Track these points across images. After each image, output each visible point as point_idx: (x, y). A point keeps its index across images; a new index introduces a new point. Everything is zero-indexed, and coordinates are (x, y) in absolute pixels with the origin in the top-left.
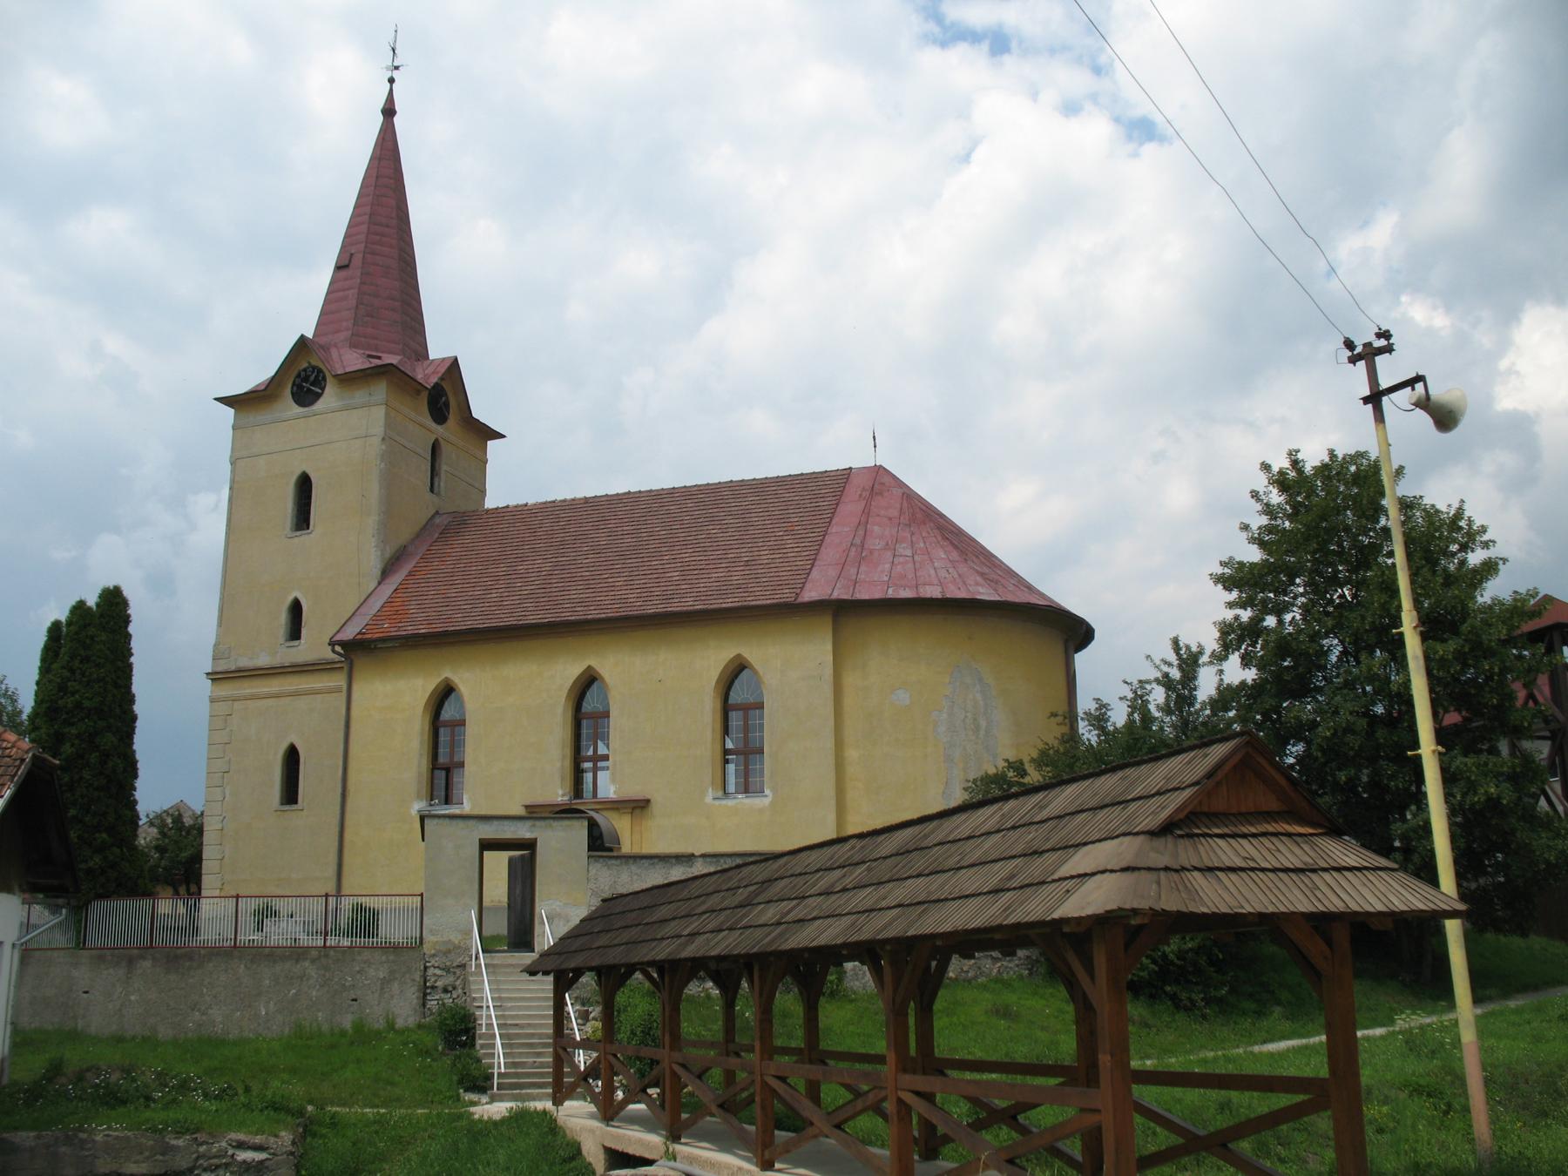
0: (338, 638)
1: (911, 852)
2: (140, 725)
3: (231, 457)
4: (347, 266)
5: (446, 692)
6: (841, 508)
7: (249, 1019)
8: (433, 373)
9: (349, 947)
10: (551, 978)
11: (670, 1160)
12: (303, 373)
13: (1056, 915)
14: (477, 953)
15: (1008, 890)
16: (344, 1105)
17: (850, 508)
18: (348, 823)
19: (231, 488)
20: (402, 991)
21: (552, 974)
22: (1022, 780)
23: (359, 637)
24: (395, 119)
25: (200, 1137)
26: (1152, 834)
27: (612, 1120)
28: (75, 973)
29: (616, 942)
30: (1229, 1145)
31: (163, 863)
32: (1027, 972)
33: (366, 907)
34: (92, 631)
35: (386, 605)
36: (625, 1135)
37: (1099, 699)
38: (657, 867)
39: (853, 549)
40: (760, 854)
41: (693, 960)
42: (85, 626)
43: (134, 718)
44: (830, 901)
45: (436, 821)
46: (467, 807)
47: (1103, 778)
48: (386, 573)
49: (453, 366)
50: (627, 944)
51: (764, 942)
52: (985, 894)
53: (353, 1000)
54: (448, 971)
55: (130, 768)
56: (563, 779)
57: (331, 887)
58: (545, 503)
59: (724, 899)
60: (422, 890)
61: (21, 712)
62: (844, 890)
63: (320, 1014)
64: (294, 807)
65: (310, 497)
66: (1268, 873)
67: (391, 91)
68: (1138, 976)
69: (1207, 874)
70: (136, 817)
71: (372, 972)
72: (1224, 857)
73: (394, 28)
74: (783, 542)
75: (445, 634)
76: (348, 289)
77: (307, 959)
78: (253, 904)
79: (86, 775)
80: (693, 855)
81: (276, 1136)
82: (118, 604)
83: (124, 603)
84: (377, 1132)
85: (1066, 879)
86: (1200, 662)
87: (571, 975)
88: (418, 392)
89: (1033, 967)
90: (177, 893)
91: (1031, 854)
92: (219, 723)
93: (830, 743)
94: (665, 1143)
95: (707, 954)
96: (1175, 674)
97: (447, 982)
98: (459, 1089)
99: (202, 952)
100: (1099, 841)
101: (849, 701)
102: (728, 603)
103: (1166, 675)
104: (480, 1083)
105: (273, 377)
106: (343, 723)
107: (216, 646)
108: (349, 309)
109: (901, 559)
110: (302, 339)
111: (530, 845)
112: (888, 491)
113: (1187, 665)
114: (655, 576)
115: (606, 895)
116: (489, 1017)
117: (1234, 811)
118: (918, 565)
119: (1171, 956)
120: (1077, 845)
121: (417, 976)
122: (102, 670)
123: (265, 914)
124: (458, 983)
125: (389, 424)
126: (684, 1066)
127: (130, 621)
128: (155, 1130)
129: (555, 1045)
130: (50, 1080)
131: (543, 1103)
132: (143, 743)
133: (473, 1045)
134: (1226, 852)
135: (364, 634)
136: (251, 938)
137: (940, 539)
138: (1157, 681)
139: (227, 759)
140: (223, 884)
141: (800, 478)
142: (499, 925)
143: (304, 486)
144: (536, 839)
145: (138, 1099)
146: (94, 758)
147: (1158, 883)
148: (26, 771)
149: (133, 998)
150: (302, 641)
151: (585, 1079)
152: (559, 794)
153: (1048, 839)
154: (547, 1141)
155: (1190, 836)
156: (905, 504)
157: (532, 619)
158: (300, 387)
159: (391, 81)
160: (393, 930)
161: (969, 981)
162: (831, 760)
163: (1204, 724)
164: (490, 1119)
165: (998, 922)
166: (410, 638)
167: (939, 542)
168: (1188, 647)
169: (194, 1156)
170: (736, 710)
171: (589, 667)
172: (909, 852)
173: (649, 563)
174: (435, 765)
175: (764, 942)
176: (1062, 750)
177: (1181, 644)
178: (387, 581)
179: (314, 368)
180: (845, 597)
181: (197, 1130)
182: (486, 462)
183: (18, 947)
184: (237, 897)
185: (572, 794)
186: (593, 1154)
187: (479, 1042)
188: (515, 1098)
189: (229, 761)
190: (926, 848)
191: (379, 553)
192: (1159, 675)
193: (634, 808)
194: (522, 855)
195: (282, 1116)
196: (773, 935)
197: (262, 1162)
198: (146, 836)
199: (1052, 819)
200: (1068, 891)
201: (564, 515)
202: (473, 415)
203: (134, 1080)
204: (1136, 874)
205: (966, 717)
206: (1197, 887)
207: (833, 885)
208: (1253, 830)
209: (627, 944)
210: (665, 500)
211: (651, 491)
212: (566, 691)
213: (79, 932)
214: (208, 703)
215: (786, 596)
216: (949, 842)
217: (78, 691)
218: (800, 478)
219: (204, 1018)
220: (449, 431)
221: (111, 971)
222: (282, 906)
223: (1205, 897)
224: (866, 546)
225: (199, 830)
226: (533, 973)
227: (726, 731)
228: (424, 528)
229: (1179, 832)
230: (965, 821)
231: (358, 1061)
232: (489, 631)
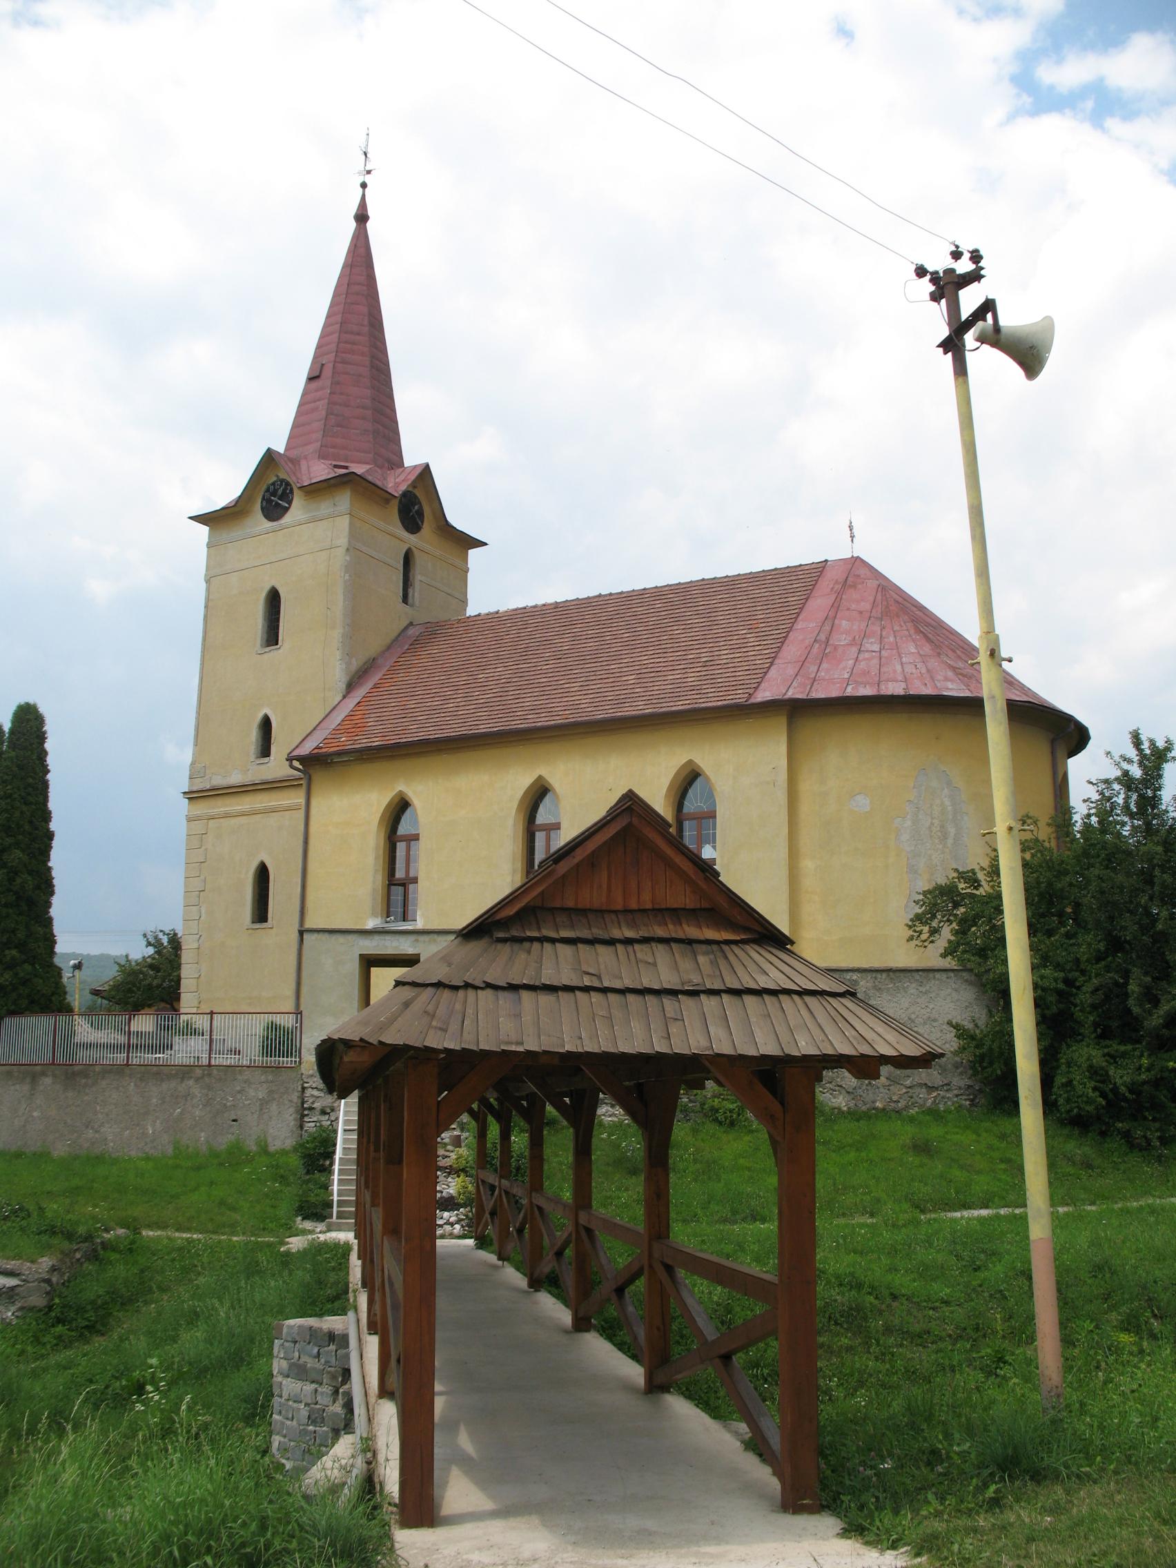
5: (401, 807)
6: (810, 603)
7: (137, 1138)
9: (248, 1067)
12: (272, 487)
17: (820, 603)
20: (280, 1112)
22: (975, 892)
23: (316, 751)
24: (368, 225)
32: (968, 1103)
33: (284, 1028)
35: (347, 718)
39: (817, 646)
43: (50, 836)
45: (315, 936)
46: (420, 924)
48: (350, 687)
49: (425, 473)
53: (234, 1121)
58: (516, 610)
63: (203, 1134)
64: (264, 925)
65: (278, 612)
71: (252, 1093)
73: (366, 132)
74: (746, 641)
75: (397, 746)
76: (319, 400)
77: (191, 1077)
88: (387, 501)
89: (975, 1097)
92: (196, 841)
93: (783, 852)
96: (1136, 772)
101: (806, 808)
103: (1126, 773)
105: (240, 497)
107: (193, 764)
109: (867, 655)
112: (863, 583)
114: (611, 680)
117: (619, 907)
118: (883, 660)
119: (1123, 1089)
121: (295, 1097)
122: (9, 787)
125: (353, 535)
127: (46, 738)
132: (59, 860)
135: (321, 748)
137: (912, 632)
138: (1117, 779)
139: (202, 877)
140: (200, 1002)
141: (773, 573)
144: (419, 955)
149: (35, 1114)
150: (272, 757)
156: (879, 597)
157: (483, 729)
158: (269, 501)
159: (364, 185)
162: (784, 872)
166: (364, 751)
167: (910, 636)
171: (540, 777)
173: (607, 668)
177: (1143, 738)
178: (351, 695)
179: (282, 481)
182: (467, 571)
184: (212, 1013)
189: (205, 881)
191: (344, 666)
192: (1119, 773)
197: (12, 1288)
201: (531, 622)
205: (932, 824)
208: (630, 934)
210: (634, 602)
211: (622, 593)
212: (517, 803)
215: (739, 697)
218: (773, 573)
219: (97, 1135)
221: (18, 1087)
229: (501, 935)
232: (445, 741)
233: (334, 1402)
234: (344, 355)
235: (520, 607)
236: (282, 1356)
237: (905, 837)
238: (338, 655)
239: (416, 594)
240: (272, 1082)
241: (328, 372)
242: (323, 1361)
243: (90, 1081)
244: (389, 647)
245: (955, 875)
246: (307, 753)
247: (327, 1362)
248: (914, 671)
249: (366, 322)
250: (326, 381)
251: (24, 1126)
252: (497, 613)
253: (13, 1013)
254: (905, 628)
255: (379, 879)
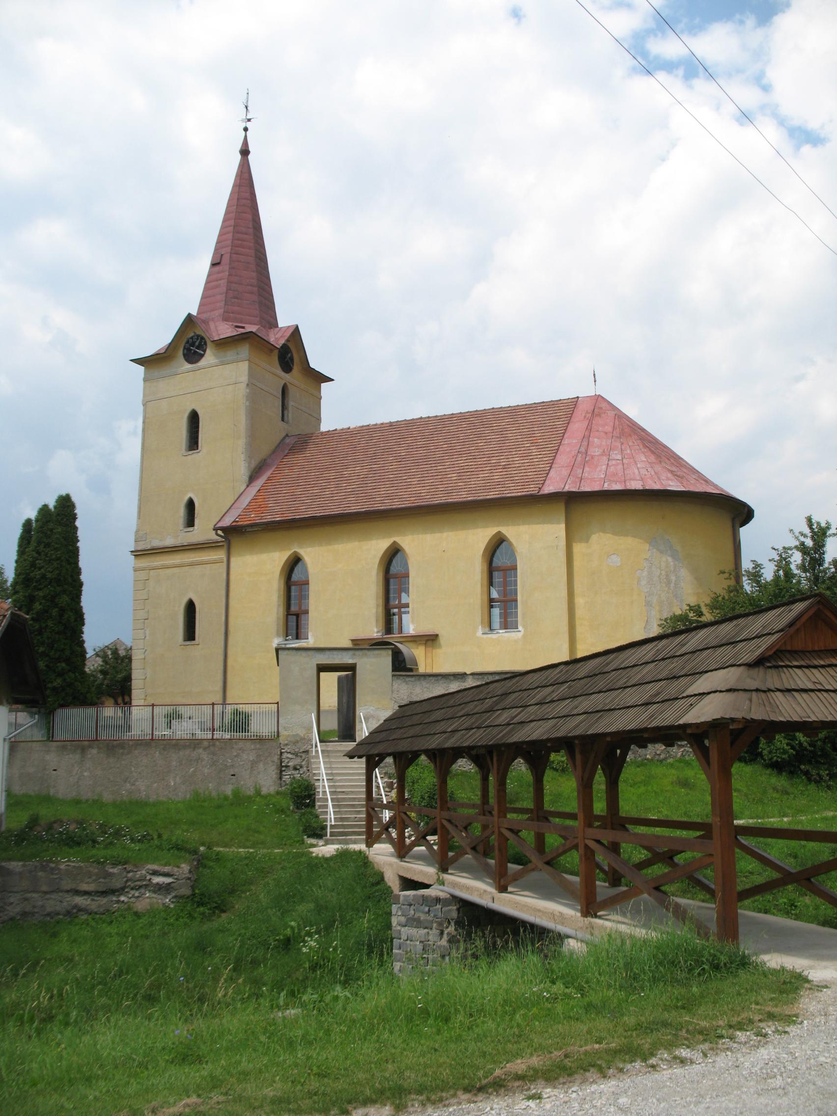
0: (220, 525)
1: (597, 675)
2: (85, 589)
3: (143, 400)
4: (218, 264)
5: (295, 561)
8: (281, 337)
10: (364, 760)
11: (440, 885)
13: (681, 722)
14: (316, 743)
15: (655, 703)
16: (225, 846)
17: (577, 426)
18: (229, 652)
19: (144, 422)
20: (265, 769)
21: (364, 758)
22: (699, 619)
23: (234, 524)
25: (129, 867)
26: (749, 665)
27: (404, 857)
28: (48, 757)
29: (405, 736)
30: (812, 880)
31: (106, 682)
34: (51, 525)
36: (412, 868)
37: (755, 561)
38: (441, 682)
39: (580, 455)
40: (506, 673)
41: (453, 749)
42: (47, 522)
43: (81, 584)
44: (543, 709)
45: (286, 652)
46: (311, 641)
47: (724, 625)
48: (252, 479)
49: (296, 333)
50: (412, 737)
51: (498, 737)
52: (639, 705)
54: (297, 756)
55: (79, 618)
56: (377, 621)
57: (218, 698)
59: (476, 706)
60: (277, 699)
61: (6, 581)
62: (552, 701)
63: (210, 785)
64: (193, 642)
65: (198, 427)
66: (830, 693)
67: (246, 137)
68: (781, 758)
69: (786, 694)
70: (84, 652)
71: (245, 756)
72: (799, 682)
73: (246, 92)
75: (294, 521)
76: (220, 280)
78: (165, 710)
79: (50, 623)
80: (465, 674)
81: (178, 867)
82: (69, 506)
83: (73, 506)
84: (247, 865)
85: (691, 696)
86: (828, 534)
87: (377, 759)
88: (271, 351)
90: (116, 703)
91: (672, 678)
93: (564, 593)
94: (437, 874)
95: (461, 745)
96: (809, 543)
97: (296, 763)
98: (303, 836)
99: (131, 743)
100: (716, 670)
102: (492, 495)
103: (803, 544)
104: (318, 832)
105: (170, 344)
106: (224, 584)
107: (137, 532)
108: (221, 294)
109: (614, 462)
110: (189, 316)
111: (352, 668)
113: (818, 536)
114: (440, 477)
115: (404, 703)
116: (324, 786)
117: (810, 649)
118: (625, 466)
120: (701, 673)
121: (276, 758)
122: (59, 552)
123: (172, 717)
124: (303, 763)
125: (251, 374)
126: (449, 821)
128: (99, 863)
129: (367, 806)
130: (31, 829)
131: (359, 845)
132: (87, 601)
133: (314, 806)
134: (801, 678)
135: (237, 522)
136: (164, 733)
137: (641, 446)
138: (796, 547)
139: (146, 610)
142: (332, 723)
143: (194, 419)
145: (88, 841)
146: (55, 612)
147: (751, 700)
148: (7, 624)
149: (86, 774)
150: (196, 527)
151: (387, 829)
152: (374, 631)
153: (683, 668)
154: (361, 871)
155: (777, 667)
156: (617, 422)
157: (354, 509)
158: (189, 350)
159: (246, 129)
160: (261, 726)
161: (661, 761)
163: (830, 578)
164: (323, 857)
165: (645, 726)
168: (818, 524)
169: (125, 879)
170: (497, 571)
171: (395, 542)
172: (596, 675)
174: (288, 612)
175: (498, 737)
176: (726, 598)
177: (813, 521)
178: (252, 485)
179: (198, 336)
180: (574, 490)
181: (126, 863)
183: (7, 741)
184: (153, 705)
185: (384, 631)
186: (392, 880)
187: (318, 804)
188: (340, 842)
189: (148, 612)
190: (607, 672)
191: (247, 465)
192: (797, 543)
193: (427, 640)
194: (347, 675)
195: (183, 853)
196: (504, 732)
197: (169, 884)
198: (92, 664)
199: (687, 654)
200: (691, 705)
202: (312, 366)
203: (85, 829)
204: (736, 693)
205: (661, 574)
206: (778, 703)
207: (545, 698)
208: (822, 663)
209: (412, 737)
213: (49, 730)
214: (132, 572)
215: (532, 490)
216: (621, 669)
217: (43, 567)
219: (133, 787)
220: (294, 378)
221: (71, 756)
222: (185, 711)
223: (783, 711)
224: (589, 453)
225: (129, 659)
226: (351, 757)
227: (491, 583)
228: (278, 446)
229: (768, 664)
230: (633, 654)
231: (236, 817)
233: (441, 939)
234: (237, 248)
235: (365, 424)
236: (400, 914)
237: (643, 582)
238: (243, 457)
239: (290, 415)
240: (259, 749)
241: (226, 260)
242: (432, 915)
243: (126, 751)
244: (274, 452)
245: (688, 608)
246: (228, 525)
247: (435, 916)
248: (647, 473)
249: (251, 226)
250: (225, 267)
251: (78, 782)
252: (349, 428)
253: (62, 706)
254: (636, 444)
255: (282, 611)
